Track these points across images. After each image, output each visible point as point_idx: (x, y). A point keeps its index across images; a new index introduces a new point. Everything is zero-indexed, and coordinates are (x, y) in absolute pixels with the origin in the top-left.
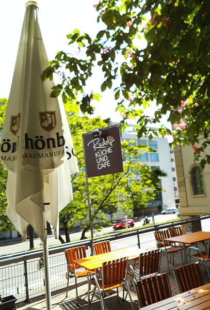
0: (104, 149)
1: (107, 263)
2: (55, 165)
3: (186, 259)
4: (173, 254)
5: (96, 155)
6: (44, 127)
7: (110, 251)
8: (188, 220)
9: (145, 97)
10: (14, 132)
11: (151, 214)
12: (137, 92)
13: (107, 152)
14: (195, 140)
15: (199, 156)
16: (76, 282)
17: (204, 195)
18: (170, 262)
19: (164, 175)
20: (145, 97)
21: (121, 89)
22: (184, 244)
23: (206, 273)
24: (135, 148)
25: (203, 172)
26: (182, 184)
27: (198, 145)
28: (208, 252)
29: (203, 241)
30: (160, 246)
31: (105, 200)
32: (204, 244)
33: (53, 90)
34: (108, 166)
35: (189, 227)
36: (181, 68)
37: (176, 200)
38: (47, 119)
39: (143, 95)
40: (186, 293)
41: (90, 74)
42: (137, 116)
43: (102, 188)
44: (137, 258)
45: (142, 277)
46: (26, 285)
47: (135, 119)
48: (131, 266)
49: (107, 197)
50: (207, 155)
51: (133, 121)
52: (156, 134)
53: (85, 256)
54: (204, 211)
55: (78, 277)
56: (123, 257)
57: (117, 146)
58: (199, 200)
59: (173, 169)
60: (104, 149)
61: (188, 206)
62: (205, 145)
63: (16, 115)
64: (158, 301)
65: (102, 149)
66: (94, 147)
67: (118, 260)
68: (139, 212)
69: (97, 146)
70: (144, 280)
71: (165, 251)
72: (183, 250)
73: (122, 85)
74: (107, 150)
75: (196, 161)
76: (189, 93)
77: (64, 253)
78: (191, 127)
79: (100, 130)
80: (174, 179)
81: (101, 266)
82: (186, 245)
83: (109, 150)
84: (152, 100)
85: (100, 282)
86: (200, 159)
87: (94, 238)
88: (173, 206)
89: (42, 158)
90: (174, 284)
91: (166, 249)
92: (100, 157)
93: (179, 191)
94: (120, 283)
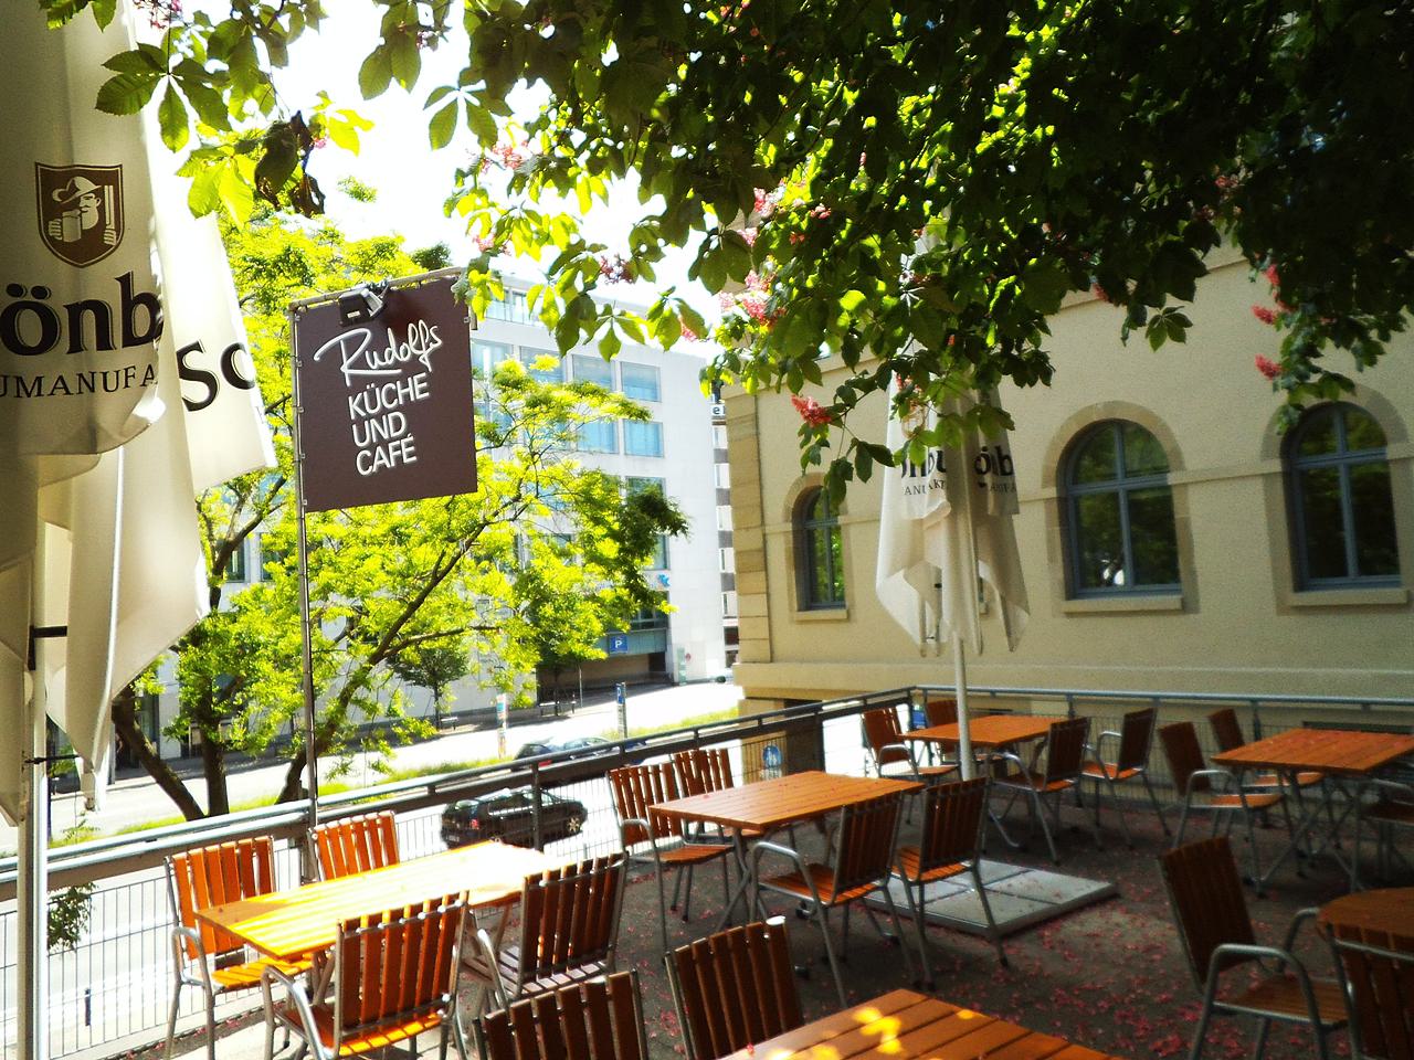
0: (392, 379)
1: (364, 925)
2: (101, 435)
3: (743, 893)
5: (353, 406)
6: (57, 246)
7: (393, 860)
8: (766, 722)
9: (586, 154)
11: (614, 688)
12: (552, 127)
13: (407, 396)
14: (804, 369)
15: (824, 443)
16: (211, 1014)
17: (841, 614)
20: (586, 154)
21: (463, 96)
22: (738, 826)
23: (826, 960)
24: (561, 395)
25: (846, 512)
26: (753, 562)
27: (821, 396)
28: (835, 863)
29: (818, 818)
30: (631, 835)
31: (403, 619)
32: (822, 829)
33: (115, 74)
34: (406, 460)
36: (755, 32)
38: (75, 204)
39: (576, 146)
42: (546, 247)
43: (401, 563)
44: (512, 899)
45: (532, 987)
47: (538, 258)
48: (482, 935)
49: (414, 607)
50: (855, 442)
51: (526, 265)
52: (630, 328)
53: (266, 887)
54: (838, 683)
55: (224, 990)
56: (443, 894)
57: (454, 368)
58: (821, 631)
60: (392, 379)
61: (772, 661)
62: (847, 396)
66: (344, 369)
67: (416, 909)
68: (564, 678)
69: (360, 363)
70: (547, 1005)
71: (651, 859)
72: (730, 855)
73: (466, 77)
74: (405, 386)
75: (811, 468)
76: (789, 160)
77: (160, 871)
78: (794, 307)
79: (377, 291)
82: (746, 832)
83: (416, 389)
84: (621, 172)
85: (323, 1015)
86: (828, 457)
87: (321, 800)
88: (712, 658)
89: (34, 398)
91: (657, 851)
92: (369, 417)
94: (423, 1018)
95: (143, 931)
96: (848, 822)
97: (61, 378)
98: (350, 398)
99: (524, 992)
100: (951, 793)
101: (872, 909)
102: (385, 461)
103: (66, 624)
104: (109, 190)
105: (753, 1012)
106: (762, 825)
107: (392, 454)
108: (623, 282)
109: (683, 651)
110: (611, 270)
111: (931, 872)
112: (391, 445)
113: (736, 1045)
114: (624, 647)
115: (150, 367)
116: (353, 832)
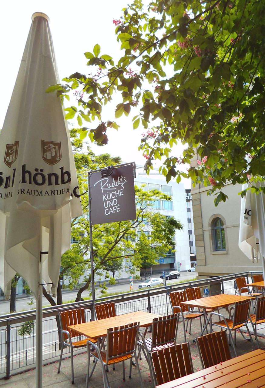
0: (114, 191)
4: (190, 321)
5: (104, 198)
6: (45, 160)
10: (9, 164)
13: (117, 195)
17: (225, 252)
18: (186, 331)
19: (179, 227)
20: (172, 133)
21: (141, 118)
22: (205, 308)
26: (200, 238)
29: (226, 307)
32: (227, 310)
35: (207, 290)
37: (191, 257)
38: (50, 150)
39: (170, 131)
40: (211, 369)
41: (110, 99)
45: (154, 349)
46: (8, 357)
57: (130, 189)
59: (189, 221)
60: (114, 191)
63: (11, 142)
64: (176, 378)
65: (111, 191)
66: (102, 188)
77: (55, 317)
80: (190, 232)
81: (152, 322)
82: (207, 310)
90: (196, 360)
92: (108, 200)
93: (196, 247)
95: (52, 332)
96: (236, 307)
97: (47, 191)
98: (103, 196)
99: (153, 350)
100: (261, 300)
101: (242, 332)
102: (112, 211)
103: (48, 251)
104: (57, 148)
105: (223, 353)
106: (212, 308)
107: (114, 210)
108: (182, 164)
109: (179, 263)
110: (179, 161)
111: (259, 321)
112: (114, 207)
113: (214, 363)
114: (163, 261)
115: (68, 189)
116: (105, 307)
